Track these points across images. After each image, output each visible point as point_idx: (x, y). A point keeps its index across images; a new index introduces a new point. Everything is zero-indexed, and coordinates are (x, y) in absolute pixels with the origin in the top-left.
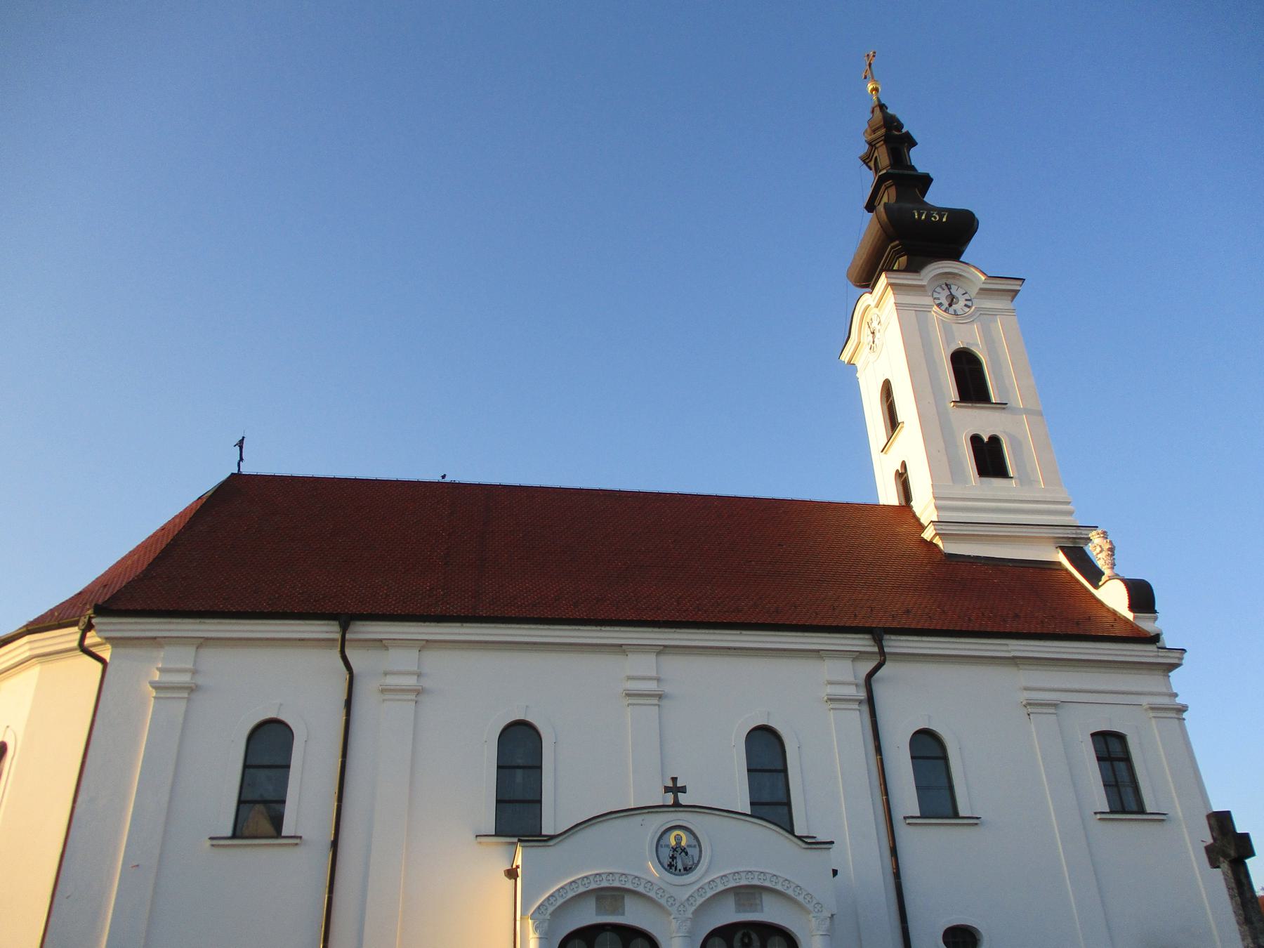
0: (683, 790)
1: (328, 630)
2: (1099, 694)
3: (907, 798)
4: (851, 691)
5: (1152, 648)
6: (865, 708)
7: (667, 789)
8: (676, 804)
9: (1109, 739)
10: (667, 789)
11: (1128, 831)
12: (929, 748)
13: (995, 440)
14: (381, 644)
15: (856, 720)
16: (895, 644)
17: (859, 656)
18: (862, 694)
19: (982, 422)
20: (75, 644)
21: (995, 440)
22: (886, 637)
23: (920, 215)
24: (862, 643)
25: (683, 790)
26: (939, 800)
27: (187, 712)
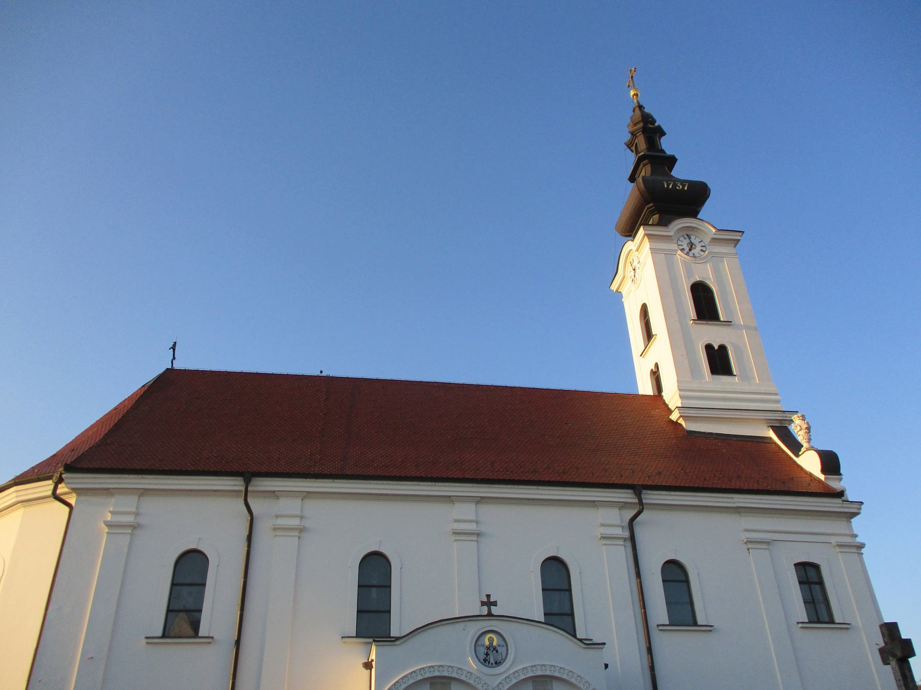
0: (495, 604)
2: (800, 537)
3: (659, 612)
4: (618, 532)
6: (629, 544)
7: (483, 604)
8: (490, 614)
10: (483, 604)
12: (675, 574)
13: (723, 348)
15: (622, 552)
16: (650, 497)
17: (624, 506)
18: (627, 534)
22: (644, 492)
25: (495, 604)
26: (683, 612)
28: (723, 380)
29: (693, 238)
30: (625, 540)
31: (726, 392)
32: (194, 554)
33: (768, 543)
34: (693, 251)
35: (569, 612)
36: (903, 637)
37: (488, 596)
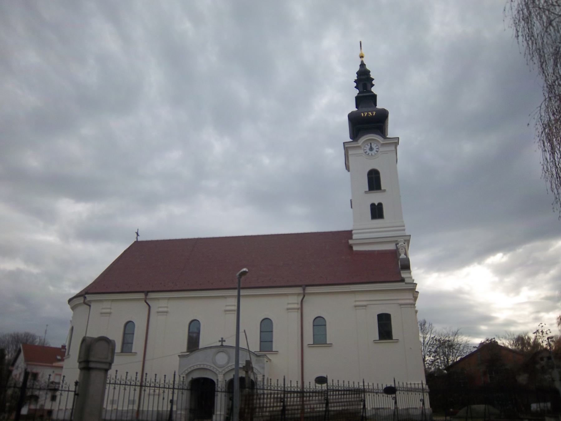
0: (225, 341)
1: (142, 296)
2: (374, 301)
3: (309, 338)
4: (296, 306)
5: (404, 283)
6: (300, 311)
7: (220, 341)
8: (222, 345)
9: (126, 332)
10: (220, 341)
11: (386, 345)
12: (320, 323)
13: (380, 205)
14: (158, 299)
15: (296, 315)
16: (309, 290)
17: (299, 294)
18: (299, 306)
19: (376, 198)
20: (82, 302)
21: (380, 205)
22: (307, 288)
23: (372, 114)
24: (299, 290)
25: (225, 341)
26: (320, 339)
27: (302, 301)
28: (378, 222)
29: (372, 144)
30: (298, 309)
31: (377, 228)
32: (192, 323)
33: (365, 306)
34: (369, 147)
35: (315, 327)
36: (358, 91)
37: (222, 338)
